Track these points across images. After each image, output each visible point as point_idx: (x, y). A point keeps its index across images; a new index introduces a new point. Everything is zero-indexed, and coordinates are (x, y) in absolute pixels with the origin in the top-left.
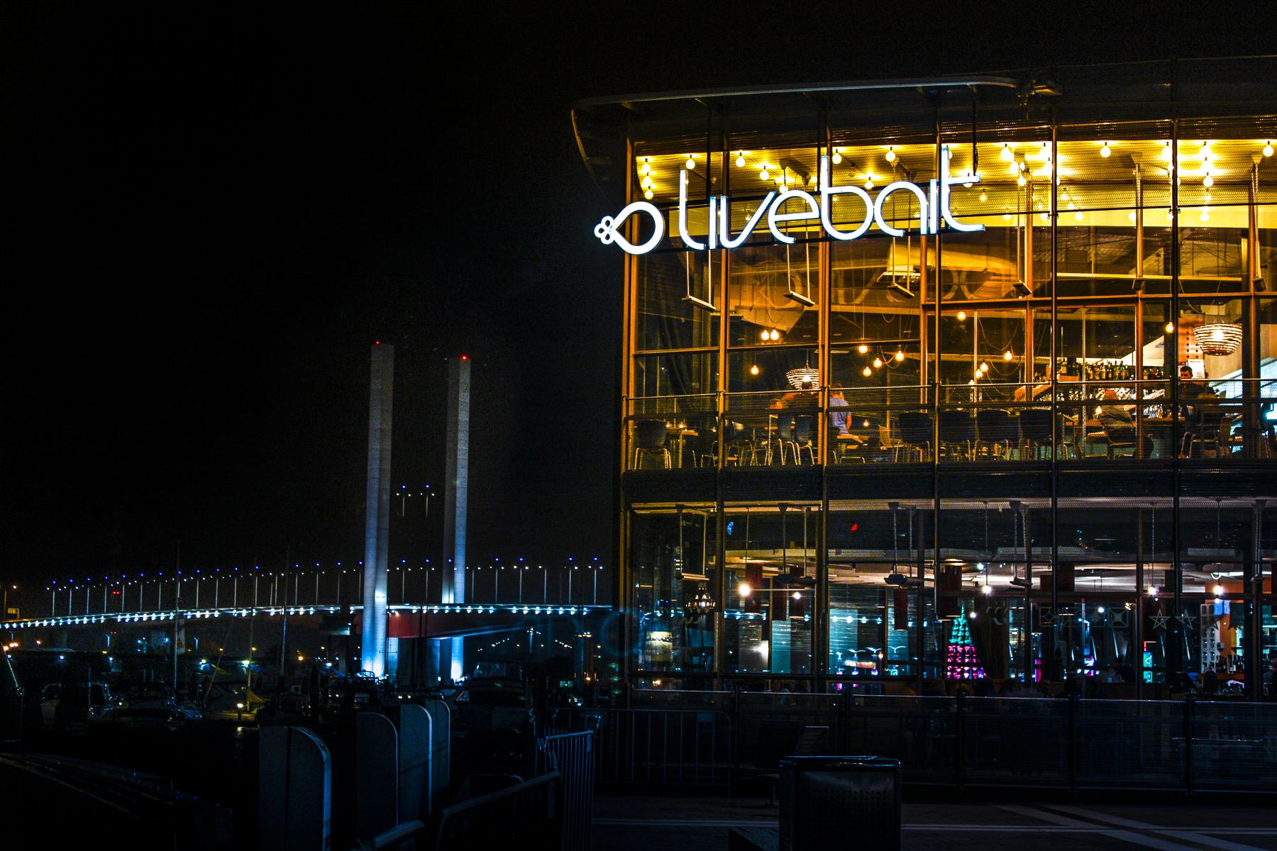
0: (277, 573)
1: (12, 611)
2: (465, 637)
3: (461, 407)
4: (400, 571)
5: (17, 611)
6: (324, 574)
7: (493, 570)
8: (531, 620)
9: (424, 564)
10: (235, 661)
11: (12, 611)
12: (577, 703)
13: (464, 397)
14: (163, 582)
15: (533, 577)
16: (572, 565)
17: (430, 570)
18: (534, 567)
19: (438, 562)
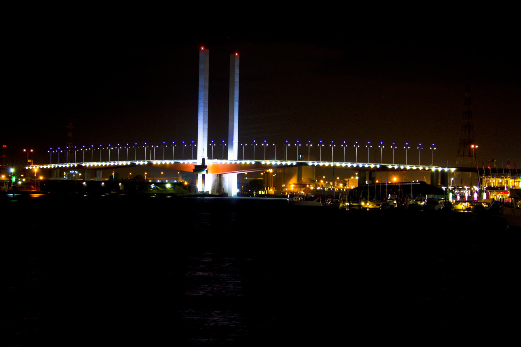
0: (155, 146)
1: (29, 161)
2: (238, 174)
3: (235, 75)
4: (211, 146)
5: (32, 161)
6: (95, 149)
7: (253, 146)
8: (270, 167)
9: (100, 147)
10: (164, 185)
11: (29, 161)
12: (64, 176)
13: (237, 71)
14: (68, 151)
15: (269, 149)
16: (287, 144)
17: (120, 148)
18: (270, 145)
19: (227, 142)
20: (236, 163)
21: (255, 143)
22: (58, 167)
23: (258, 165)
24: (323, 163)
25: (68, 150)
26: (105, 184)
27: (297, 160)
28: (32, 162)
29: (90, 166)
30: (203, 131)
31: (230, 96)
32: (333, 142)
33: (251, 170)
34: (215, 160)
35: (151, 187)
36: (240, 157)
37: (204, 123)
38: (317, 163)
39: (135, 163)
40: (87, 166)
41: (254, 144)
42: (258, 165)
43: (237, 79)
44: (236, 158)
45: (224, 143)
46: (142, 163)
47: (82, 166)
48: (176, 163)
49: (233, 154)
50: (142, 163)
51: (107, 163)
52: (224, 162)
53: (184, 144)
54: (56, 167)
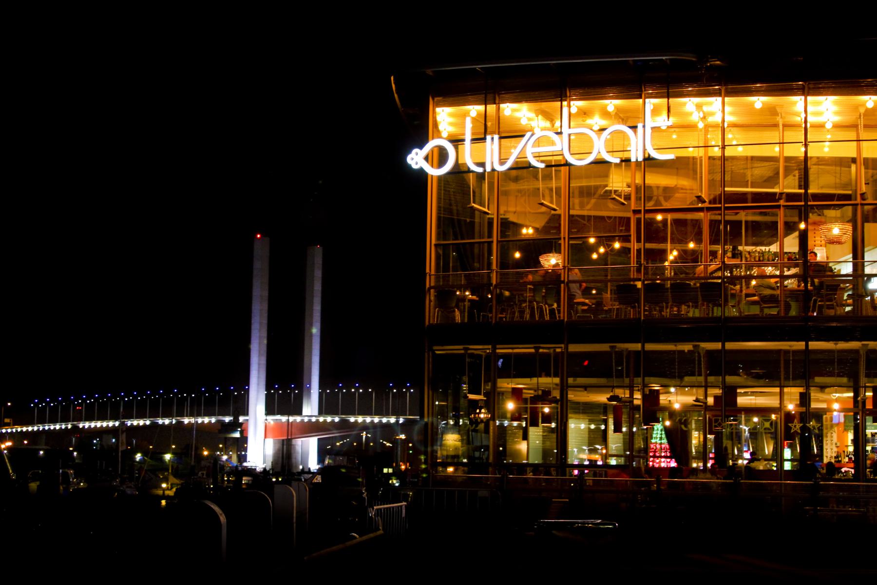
1: (7, 420)
2: (318, 439)
5: (10, 421)
13: (318, 274)
20: (310, 421)
21: (342, 388)
22: (44, 429)
23: (344, 424)
24: (355, 417)
25: (150, 395)
26: (45, 453)
27: (406, 415)
28: (12, 422)
29: (102, 426)
30: (257, 369)
31: (307, 313)
32: (207, 395)
33: (345, 430)
34: (278, 417)
35: (135, 458)
36: (321, 412)
37: (260, 355)
38: (371, 418)
39: (183, 421)
40: (86, 427)
41: (341, 389)
42: (344, 424)
43: (318, 287)
44: (316, 413)
45: (295, 389)
46: (167, 421)
47: (78, 427)
48: (218, 421)
49: (310, 409)
50: (167, 421)
51: (139, 421)
52: (298, 419)
53: (234, 391)
54: (41, 430)
